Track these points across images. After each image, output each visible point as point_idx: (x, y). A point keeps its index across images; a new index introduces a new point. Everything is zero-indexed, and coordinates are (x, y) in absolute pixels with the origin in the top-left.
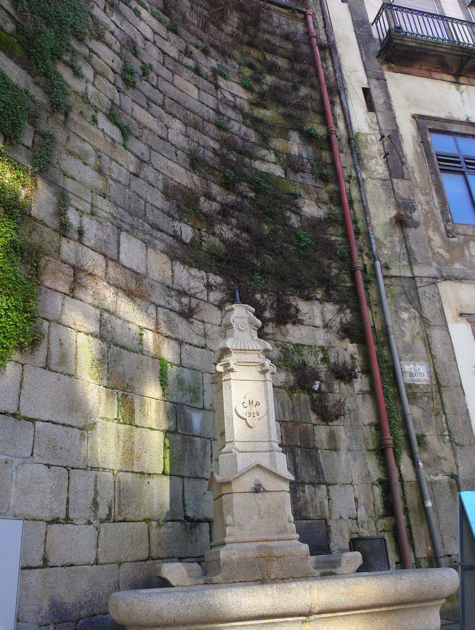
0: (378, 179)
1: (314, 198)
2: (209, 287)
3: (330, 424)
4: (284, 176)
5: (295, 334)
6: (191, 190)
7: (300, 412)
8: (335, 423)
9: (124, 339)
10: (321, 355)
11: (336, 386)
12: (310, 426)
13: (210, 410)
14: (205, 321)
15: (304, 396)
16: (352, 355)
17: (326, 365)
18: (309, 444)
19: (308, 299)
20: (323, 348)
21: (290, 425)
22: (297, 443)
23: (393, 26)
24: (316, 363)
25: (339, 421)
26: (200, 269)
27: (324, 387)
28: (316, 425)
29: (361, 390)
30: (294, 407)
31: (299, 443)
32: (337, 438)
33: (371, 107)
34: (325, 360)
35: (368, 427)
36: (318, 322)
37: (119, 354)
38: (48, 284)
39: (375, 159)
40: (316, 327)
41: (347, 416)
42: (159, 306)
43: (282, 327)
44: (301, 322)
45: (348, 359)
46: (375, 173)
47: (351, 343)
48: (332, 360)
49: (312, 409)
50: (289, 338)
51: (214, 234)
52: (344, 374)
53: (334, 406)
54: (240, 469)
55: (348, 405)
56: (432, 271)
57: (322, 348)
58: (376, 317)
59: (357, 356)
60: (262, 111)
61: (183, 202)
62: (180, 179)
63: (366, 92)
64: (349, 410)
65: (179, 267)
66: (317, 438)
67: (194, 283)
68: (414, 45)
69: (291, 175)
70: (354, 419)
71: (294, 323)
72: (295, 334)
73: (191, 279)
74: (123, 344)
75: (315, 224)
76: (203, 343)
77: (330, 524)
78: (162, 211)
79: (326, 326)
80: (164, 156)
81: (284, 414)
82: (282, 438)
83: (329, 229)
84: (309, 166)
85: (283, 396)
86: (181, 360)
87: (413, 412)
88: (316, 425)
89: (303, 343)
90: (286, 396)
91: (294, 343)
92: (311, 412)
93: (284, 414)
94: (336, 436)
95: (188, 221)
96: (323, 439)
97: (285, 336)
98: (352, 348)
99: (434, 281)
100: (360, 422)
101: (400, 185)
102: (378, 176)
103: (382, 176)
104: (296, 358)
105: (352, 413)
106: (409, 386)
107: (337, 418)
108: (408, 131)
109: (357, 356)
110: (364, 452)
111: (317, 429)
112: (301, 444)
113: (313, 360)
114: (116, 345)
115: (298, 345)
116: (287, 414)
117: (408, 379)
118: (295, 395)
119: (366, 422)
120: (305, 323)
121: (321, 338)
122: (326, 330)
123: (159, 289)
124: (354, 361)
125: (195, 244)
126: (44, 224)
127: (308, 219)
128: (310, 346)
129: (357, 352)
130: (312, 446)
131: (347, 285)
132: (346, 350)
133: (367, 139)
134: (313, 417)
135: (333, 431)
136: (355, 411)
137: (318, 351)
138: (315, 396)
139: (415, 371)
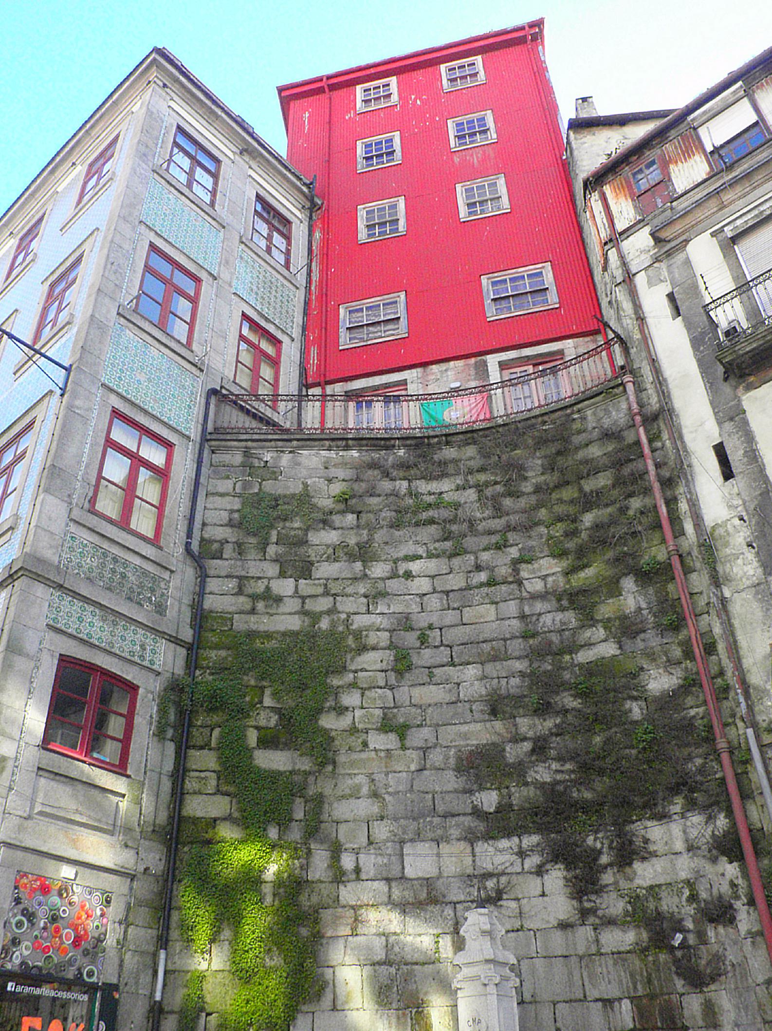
0: (748, 587)
1: (662, 663)
2: (522, 854)
3: (705, 990)
4: (618, 652)
5: (646, 873)
6: (493, 744)
7: (659, 980)
8: (712, 987)
9: (416, 955)
10: (687, 893)
11: (711, 933)
12: (674, 998)
13: (530, 1003)
14: (520, 896)
15: (663, 957)
16: (732, 881)
17: (695, 905)
18: (674, 1023)
19: (663, 817)
20: (689, 882)
21: (644, 1001)
22: (656, 1023)
24: (680, 906)
25: (718, 983)
26: (509, 836)
27: (692, 940)
28: (684, 994)
29: (749, 932)
30: (651, 974)
31: (659, 1024)
32: (716, 1010)
34: (693, 898)
35: (764, 987)
36: (679, 846)
37: (410, 973)
38: (329, 934)
39: (741, 556)
40: (676, 853)
41: (730, 975)
42: (458, 903)
43: (628, 870)
44: (654, 854)
45: (725, 889)
46: (744, 580)
47: (731, 863)
48: (704, 895)
49: (677, 974)
50: (638, 882)
51: (526, 784)
52: (720, 913)
53: (709, 963)
55: (731, 956)
57: (688, 883)
58: (763, 812)
59: (740, 881)
60: (582, 574)
61: (481, 766)
62: (477, 739)
63: (720, 450)
64: (733, 965)
65: (481, 847)
66: (686, 1013)
67: (499, 859)
68: (755, 345)
69: (628, 645)
70: (742, 977)
71: (644, 859)
72: (646, 873)
73: (497, 855)
74: (415, 960)
75: (670, 701)
76: (517, 925)
78: (456, 791)
79: (691, 848)
80: (455, 724)
81: (635, 988)
82: (634, 1020)
83: (686, 701)
84: (651, 619)
85: (633, 963)
88: (684, 994)
89: (658, 883)
90: (637, 962)
91: (645, 885)
92: (675, 977)
93: (635, 988)
94: (716, 1006)
95: (492, 785)
96: (695, 1013)
97: (631, 880)
98: (732, 870)
100: (750, 981)
102: (748, 582)
103: (755, 578)
104: (652, 905)
105: (737, 969)
107: (713, 980)
109: (740, 881)
110: (759, 1026)
111: (685, 999)
112: (662, 1025)
113: (669, 903)
114: (406, 964)
115: (651, 887)
116: (639, 986)
118: (650, 958)
119: (761, 979)
120: (659, 853)
121: (684, 867)
122: (691, 854)
123: (456, 884)
124: (735, 889)
125: (503, 809)
126: (322, 882)
127: (656, 699)
128: (670, 884)
129: (739, 874)
130: (680, 1025)
131: (717, 776)
132: (723, 875)
133: (726, 531)
134: (679, 984)
135: (710, 1000)
136: (741, 968)
137: (683, 887)
138: (679, 954)
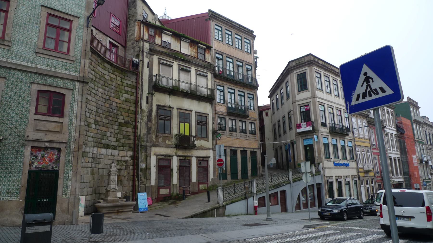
23: (104, 211)
33: (147, 102)
54: (123, 56)
56: (151, 145)
63: (147, 97)
77: (168, 105)
86: (78, 81)
87: (140, 173)
99: (151, 147)
101: (149, 124)
106: (141, 168)
108: (154, 109)
117: (141, 167)
139: (143, 166)
